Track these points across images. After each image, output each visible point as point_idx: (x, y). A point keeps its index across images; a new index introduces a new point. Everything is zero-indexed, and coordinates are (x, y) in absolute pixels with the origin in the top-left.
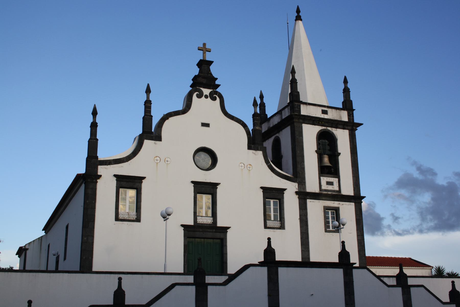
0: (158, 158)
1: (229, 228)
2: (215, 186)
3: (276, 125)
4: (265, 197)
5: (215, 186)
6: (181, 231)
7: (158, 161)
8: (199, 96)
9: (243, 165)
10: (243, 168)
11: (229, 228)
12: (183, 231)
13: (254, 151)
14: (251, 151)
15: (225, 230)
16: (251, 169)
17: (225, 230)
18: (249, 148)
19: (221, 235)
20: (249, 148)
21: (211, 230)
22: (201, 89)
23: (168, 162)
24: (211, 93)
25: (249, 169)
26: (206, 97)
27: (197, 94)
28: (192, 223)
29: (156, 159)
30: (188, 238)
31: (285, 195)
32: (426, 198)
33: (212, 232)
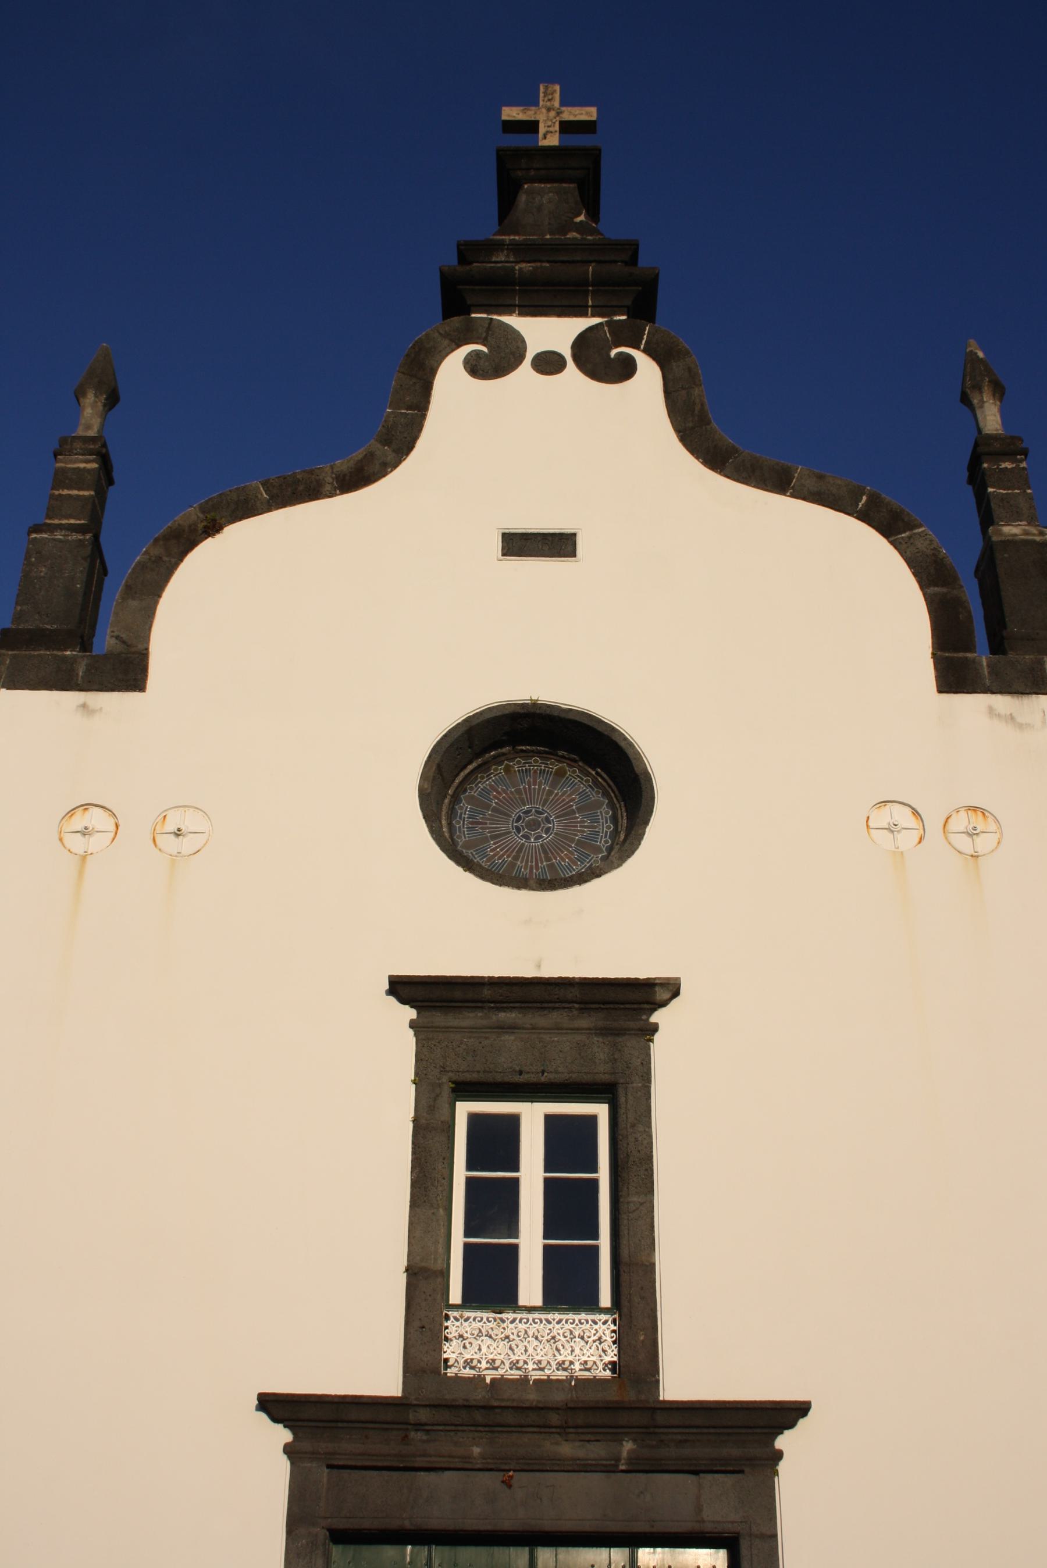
0: (96, 819)
1: (790, 1413)
2: (628, 1006)
3: (459, 315)
4: (440, 1083)
5: (628, 1006)
6: (264, 1464)
7: (95, 843)
8: (498, 360)
9: (903, 816)
10: (907, 840)
11: (790, 1413)
12: (282, 1468)
13: (1002, 702)
14: (972, 707)
15: (748, 1435)
16: (984, 844)
17: (748, 1435)
18: (954, 676)
19: (717, 1499)
20: (954, 676)
21: (596, 1451)
22: (507, 319)
23: (187, 844)
24: (582, 345)
25: (964, 843)
26: (549, 364)
27: (477, 354)
28: (381, 1376)
29: (79, 821)
30: (340, 1537)
31: (659, 1047)
32: (161, 543)
33: (609, 1468)
